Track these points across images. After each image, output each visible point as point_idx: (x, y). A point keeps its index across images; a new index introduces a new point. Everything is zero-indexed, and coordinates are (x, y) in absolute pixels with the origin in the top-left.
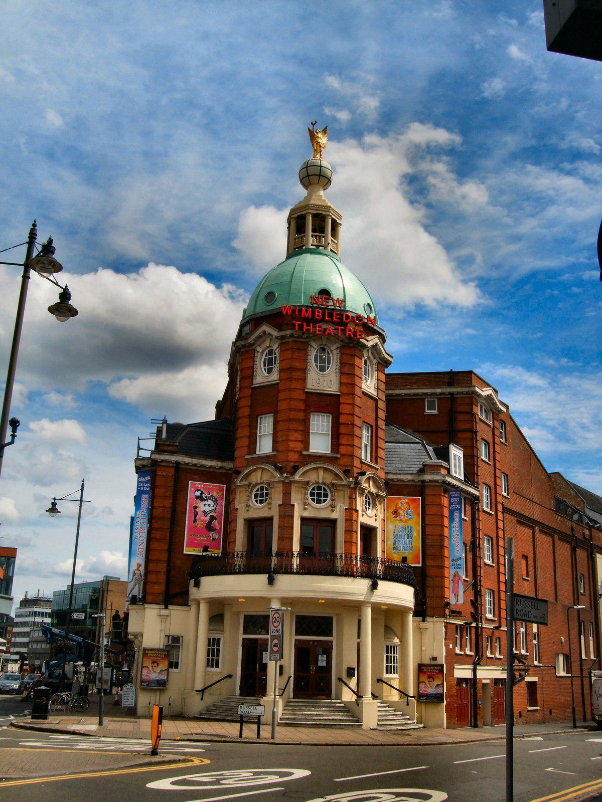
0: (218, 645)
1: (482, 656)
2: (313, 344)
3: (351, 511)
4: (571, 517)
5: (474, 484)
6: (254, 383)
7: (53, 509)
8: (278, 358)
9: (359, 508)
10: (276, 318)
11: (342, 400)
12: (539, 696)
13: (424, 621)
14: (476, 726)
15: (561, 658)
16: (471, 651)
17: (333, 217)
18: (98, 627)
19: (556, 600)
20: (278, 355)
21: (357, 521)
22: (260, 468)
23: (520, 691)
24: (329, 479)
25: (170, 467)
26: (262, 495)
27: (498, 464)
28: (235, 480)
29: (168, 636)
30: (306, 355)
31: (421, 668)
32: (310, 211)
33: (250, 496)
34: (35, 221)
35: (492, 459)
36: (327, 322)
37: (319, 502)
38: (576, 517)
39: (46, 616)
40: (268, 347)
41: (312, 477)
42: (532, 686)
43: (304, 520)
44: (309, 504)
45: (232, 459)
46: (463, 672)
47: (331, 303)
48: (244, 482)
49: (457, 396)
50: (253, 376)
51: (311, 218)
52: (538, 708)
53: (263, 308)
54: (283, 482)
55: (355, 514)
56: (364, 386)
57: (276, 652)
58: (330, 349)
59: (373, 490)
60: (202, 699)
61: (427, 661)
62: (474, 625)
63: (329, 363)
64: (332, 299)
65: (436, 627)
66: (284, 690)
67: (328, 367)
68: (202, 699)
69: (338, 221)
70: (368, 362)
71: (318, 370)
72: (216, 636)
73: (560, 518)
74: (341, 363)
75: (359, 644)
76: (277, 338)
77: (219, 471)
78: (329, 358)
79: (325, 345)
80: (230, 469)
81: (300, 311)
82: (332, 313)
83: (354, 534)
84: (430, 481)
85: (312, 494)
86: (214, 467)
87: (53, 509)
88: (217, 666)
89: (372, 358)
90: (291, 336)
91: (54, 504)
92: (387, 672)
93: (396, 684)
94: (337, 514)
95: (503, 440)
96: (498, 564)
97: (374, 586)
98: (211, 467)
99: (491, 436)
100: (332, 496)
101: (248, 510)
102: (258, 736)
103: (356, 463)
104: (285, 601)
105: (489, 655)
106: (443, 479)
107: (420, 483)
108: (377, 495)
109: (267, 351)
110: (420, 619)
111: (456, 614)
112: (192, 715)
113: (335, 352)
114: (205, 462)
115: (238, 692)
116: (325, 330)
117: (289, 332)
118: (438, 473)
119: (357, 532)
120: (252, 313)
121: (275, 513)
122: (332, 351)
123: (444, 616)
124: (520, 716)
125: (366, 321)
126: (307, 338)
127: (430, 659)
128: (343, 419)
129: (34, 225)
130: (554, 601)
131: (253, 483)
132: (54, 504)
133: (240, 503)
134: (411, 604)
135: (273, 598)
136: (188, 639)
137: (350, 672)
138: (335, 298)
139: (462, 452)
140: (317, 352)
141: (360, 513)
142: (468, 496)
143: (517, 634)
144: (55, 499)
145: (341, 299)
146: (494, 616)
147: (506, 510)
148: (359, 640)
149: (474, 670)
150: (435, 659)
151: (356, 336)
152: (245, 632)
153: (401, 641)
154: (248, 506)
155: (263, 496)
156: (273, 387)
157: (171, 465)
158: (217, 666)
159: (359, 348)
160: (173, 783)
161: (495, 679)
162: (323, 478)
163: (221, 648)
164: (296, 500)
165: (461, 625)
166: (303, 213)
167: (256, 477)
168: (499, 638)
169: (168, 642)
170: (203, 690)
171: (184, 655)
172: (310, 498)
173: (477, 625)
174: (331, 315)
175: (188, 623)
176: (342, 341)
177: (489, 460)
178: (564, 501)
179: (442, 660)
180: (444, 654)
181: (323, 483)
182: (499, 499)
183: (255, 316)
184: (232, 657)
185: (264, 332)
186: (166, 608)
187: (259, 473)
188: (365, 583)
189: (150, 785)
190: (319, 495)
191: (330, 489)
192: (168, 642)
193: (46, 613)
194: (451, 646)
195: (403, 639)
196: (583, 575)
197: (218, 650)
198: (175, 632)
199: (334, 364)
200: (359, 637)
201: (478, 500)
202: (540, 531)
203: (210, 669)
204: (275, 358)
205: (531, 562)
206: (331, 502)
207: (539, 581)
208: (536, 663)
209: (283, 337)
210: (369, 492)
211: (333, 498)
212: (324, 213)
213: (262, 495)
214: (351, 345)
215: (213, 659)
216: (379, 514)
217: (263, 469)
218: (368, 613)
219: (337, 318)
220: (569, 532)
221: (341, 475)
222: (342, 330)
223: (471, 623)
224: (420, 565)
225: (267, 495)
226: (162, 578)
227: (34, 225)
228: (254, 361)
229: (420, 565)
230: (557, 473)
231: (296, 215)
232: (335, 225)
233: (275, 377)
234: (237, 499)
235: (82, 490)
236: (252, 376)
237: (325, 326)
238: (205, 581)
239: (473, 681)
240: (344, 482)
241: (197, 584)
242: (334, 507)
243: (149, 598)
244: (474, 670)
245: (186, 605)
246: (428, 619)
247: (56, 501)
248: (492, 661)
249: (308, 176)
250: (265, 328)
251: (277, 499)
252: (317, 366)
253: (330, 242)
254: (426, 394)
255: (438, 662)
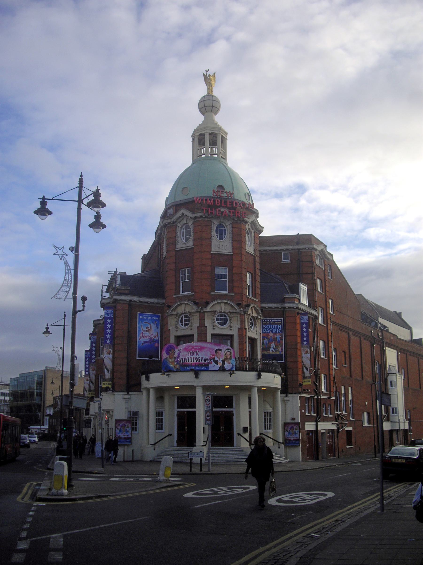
0: (162, 416)
1: (321, 416)
2: (215, 221)
3: (242, 330)
4: (370, 324)
5: (314, 309)
6: (177, 247)
7: (47, 332)
8: (192, 231)
9: (247, 327)
10: (189, 204)
11: (234, 258)
12: (353, 439)
13: (287, 396)
14: (317, 459)
15: (365, 414)
16: (314, 413)
17: (222, 135)
18: (42, 401)
19: (362, 378)
20: (192, 229)
21: (246, 335)
22: (184, 303)
23: (343, 438)
24: (228, 309)
25: (125, 303)
26: (185, 321)
27: (327, 294)
28: (168, 311)
29: (130, 412)
30: (211, 229)
31: (286, 425)
32: (207, 131)
33: (178, 322)
34: (81, 173)
35: (324, 291)
36: (223, 207)
37: (222, 324)
38: (373, 324)
39: (6, 396)
40: (185, 224)
41: (217, 308)
42: (349, 432)
43: (213, 335)
44: (216, 326)
45: (163, 297)
46: (310, 426)
47: (225, 195)
48: (174, 312)
49: (303, 251)
50: (176, 243)
51: (208, 135)
52: (353, 446)
53: (181, 198)
54: (199, 312)
55: (244, 330)
56: (247, 248)
57: (208, 420)
58: (225, 224)
59: (255, 315)
60: (154, 450)
61: (289, 421)
62: (316, 397)
63: (225, 234)
64: (226, 192)
65: (295, 401)
66: (207, 442)
67: (224, 237)
68: (154, 450)
69: (225, 137)
70: (248, 232)
71: (218, 239)
72: (160, 410)
73: (364, 326)
74: (233, 234)
75: (250, 413)
76: (191, 218)
77: (156, 305)
78: (225, 230)
79: (223, 222)
80: (163, 304)
81: (206, 200)
82: (227, 201)
83: (245, 344)
84: (289, 308)
85: (217, 320)
86: (153, 303)
87: (47, 332)
88: (162, 429)
89: (251, 229)
90: (201, 217)
91: (47, 328)
92: (265, 429)
93: (271, 435)
94: (235, 332)
95: (330, 278)
96: (329, 358)
97: (259, 376)
98: (151, 303)
99: (323, 275)
100: (230, 320)
101: (177, 331)
102: (201, 470)
103: (244, 298)
104: (205, 388)
105: (325, 416)
106: (297, 306)
107: (282, 309)
108: (257, 318)
109: (184, 226)
110: (285, 395)
111: (304, 391)
112: (149, 460)
113: (229, 226)
114: (147, 300)
115: (175, 444)
116: (223, 212)
117: (199, 214)
118: (293, 302)
119: (246, 343)
120: (173, 201)
121: (195, 332)
122: (227, 226)
123: (299, 392)
124: (343, 451)
125: (248, 206)
126: (212, 217)
127: (291, 419)
128: (235, 270)
129: (81, 176)
130: (361, 379)
131: (180, 313)
132: (47, 328)
133: (171, 326)
134: (280, 387)
135: (197, 386)
136: (143, 411)
137: (245, 430)
138: (228, 191)
139: (306, 288)
140: (217, 227)
141: (247, 330)
142: (311, 316)
143: (340, 401)
144: (47, 325)
145: (231, 192)
146: (327, 391)
147: (334, 323)
148: (250, 410)
149: (317, 426)
150: (294, 419)
151: (242, 216)
152: (178, 407)
153: (273, 409)
154: (177, 328)
155: (186, 320)
156: (190, 250)
157: (126, 302)
158: (162, 429)
159: (244, 223)
160: (193, 494)
161: (195, 397)
162: (224, 309)
163: (164, 418)
164: (208, 323)
165: (308, 398)
166: (203, 132)
167: (181, 310)
168: (330, 405)
169: (130, 415)
170: (155, 444)
171: (142, 423)
172: (216, 322)
173: (318, 397)
174: (226, 202)
175: (143, 403)
176: (234, 219)
177: (322, 292)
178: (365, 313)
179: (298, 420)
180: (300, 416)
181: (224, 312)
182: (329, 316)
183: (176, 203)
184: (171, 423)
185: (183, 214)
186: (128, 394)
187: (183, 306)
188: (254, 374)
189: (185, 495)
190: (222, 320)
191: (229, 316)
192: (130, 415)
193: (7, 393)
194: (303, 410)
195: (274, 407)
196: (378, 361)
197: (162, 419)
198: (134, 409)
199: (228, 235)
200: (250, 407)
201: (317, 318)
202: (353, 334)
203: (157, 431)
204: (190, 231)
205: (347, 356)
206: (229, 325)
207: (353, 367)
208: (351, 419)
209: (196, 218)
210: (252, 317)
211: (231, 321)
212: (216, 132)
213: (185, 321)
214: (239, 222)
215: (159, 425)
216: (258, 330)
217: (186, 304)
218: (255, 394)
219: (229, 205)
220: (370, 335)
221: (235, 306)
222: (233, 212)
223: (314, 396)
224: (284, 361)
225: (189, 320)
226: (124, 374)
227: (81, 176)
228: (176, 233)
229: (284, 361)
230: (360, 294)
231: (198, 134)
232: (224, 140)
233: (191, 244)
234: (169, 323)
235: (65, 319)
236: (175, 243)
237: (222, 210)
238: (152, 376)
239: (316, 431)
240: (238, 311)
241: (148, 379)
242: (232, 327)
243: (116, 388)
244: (317, 426)
245: (140, 391)
246: (289, 395)
247: (48, 326)
248: (327, 419)
249: (205, 107)
250: (183, 211)
251: (196, 323)
252: (217, 236)
253: (221, 152)
254: (283, 250)
255: (296, 421)
